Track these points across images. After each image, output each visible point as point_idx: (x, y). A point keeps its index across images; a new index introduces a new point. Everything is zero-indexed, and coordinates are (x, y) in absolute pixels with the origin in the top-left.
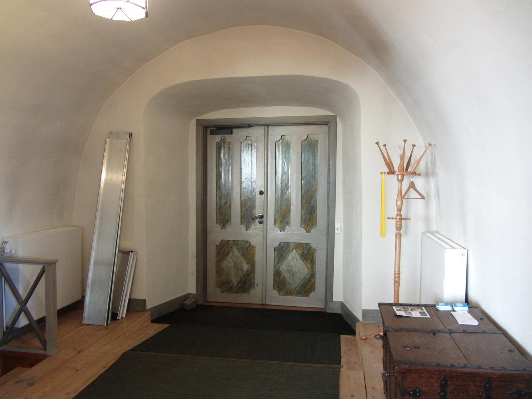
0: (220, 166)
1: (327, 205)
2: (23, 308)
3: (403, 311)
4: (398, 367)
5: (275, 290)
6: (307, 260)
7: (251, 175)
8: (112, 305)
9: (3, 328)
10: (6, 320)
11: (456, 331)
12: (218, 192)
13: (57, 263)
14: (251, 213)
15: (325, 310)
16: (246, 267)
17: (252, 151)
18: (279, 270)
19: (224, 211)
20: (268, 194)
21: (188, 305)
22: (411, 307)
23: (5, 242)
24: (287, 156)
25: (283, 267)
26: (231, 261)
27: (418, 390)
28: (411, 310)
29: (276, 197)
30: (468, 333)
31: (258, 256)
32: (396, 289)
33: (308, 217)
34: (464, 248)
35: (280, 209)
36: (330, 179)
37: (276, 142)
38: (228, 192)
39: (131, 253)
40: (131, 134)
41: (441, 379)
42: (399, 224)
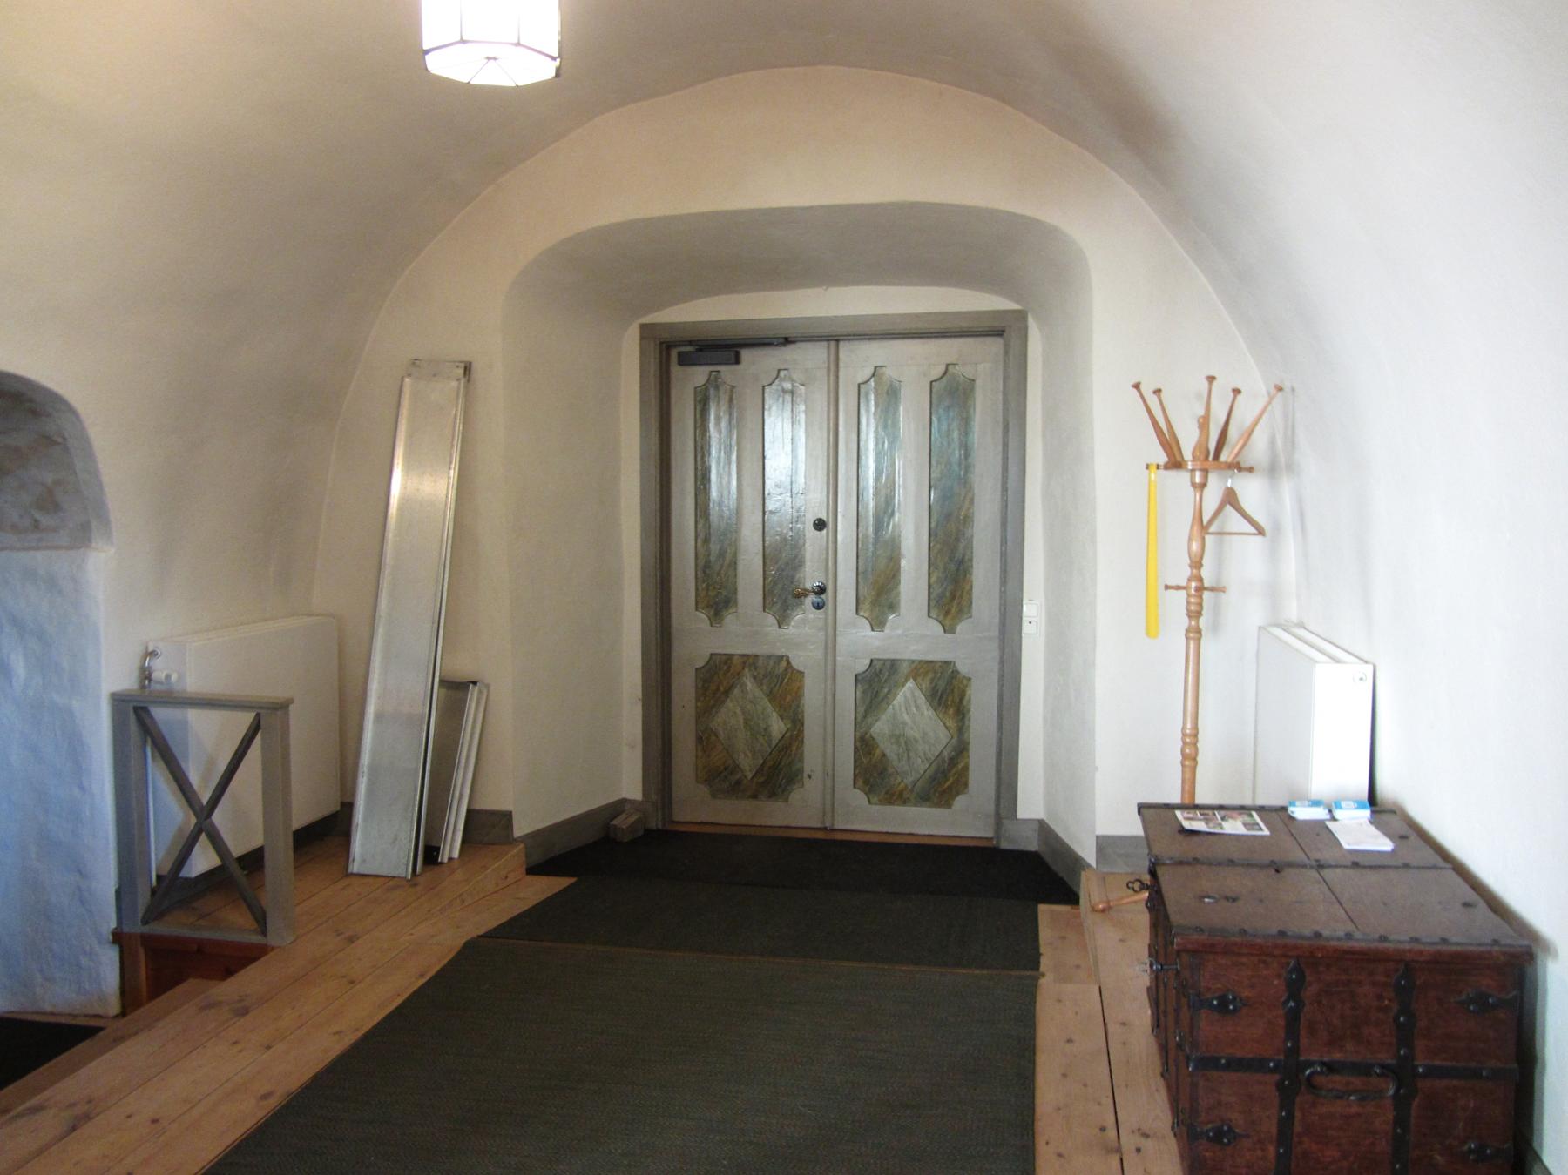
0: (705, 452)
1: (1001, 556)
2: (203, 826)
3: (1200, 820)
4: (1182, 939)
5: (859, 789)
6: (946, 707)
7: (792, 476)
8: (427, 823)
9: (151, 880)
10: (156, 859)
11: (1333, 864)
12: (701, 522)
13: (292, 707)
14: (792, 579)
15: (994, 842)
16: (777, 727)
17: (794, 410)
18: (868, 735)
19: (718, 574)
20: (839, 528)
21: (623, 829)
22: (1223, 813)
23: (153, 654)
24: (890, 422)
25: (880, 727)
26: (738, 711)
27: (1231, 997)
28: (1223, 819)
29: (860, 536)
30: (1365, 867)
31: (812, 699)
32: (1188, 776)
33: (949, 588)
34: (1366, 662)
35: (870, 570)
36: (1009, 486)
37: (859, 385)
38: (727, 524)
39: (471, 686)
40: (468, 365)
41: (1289, 969)
42: (1194, 603)
